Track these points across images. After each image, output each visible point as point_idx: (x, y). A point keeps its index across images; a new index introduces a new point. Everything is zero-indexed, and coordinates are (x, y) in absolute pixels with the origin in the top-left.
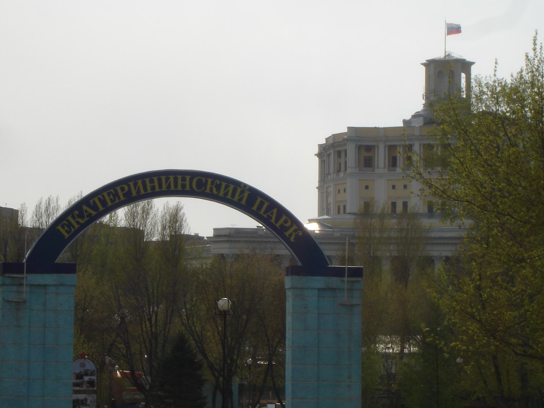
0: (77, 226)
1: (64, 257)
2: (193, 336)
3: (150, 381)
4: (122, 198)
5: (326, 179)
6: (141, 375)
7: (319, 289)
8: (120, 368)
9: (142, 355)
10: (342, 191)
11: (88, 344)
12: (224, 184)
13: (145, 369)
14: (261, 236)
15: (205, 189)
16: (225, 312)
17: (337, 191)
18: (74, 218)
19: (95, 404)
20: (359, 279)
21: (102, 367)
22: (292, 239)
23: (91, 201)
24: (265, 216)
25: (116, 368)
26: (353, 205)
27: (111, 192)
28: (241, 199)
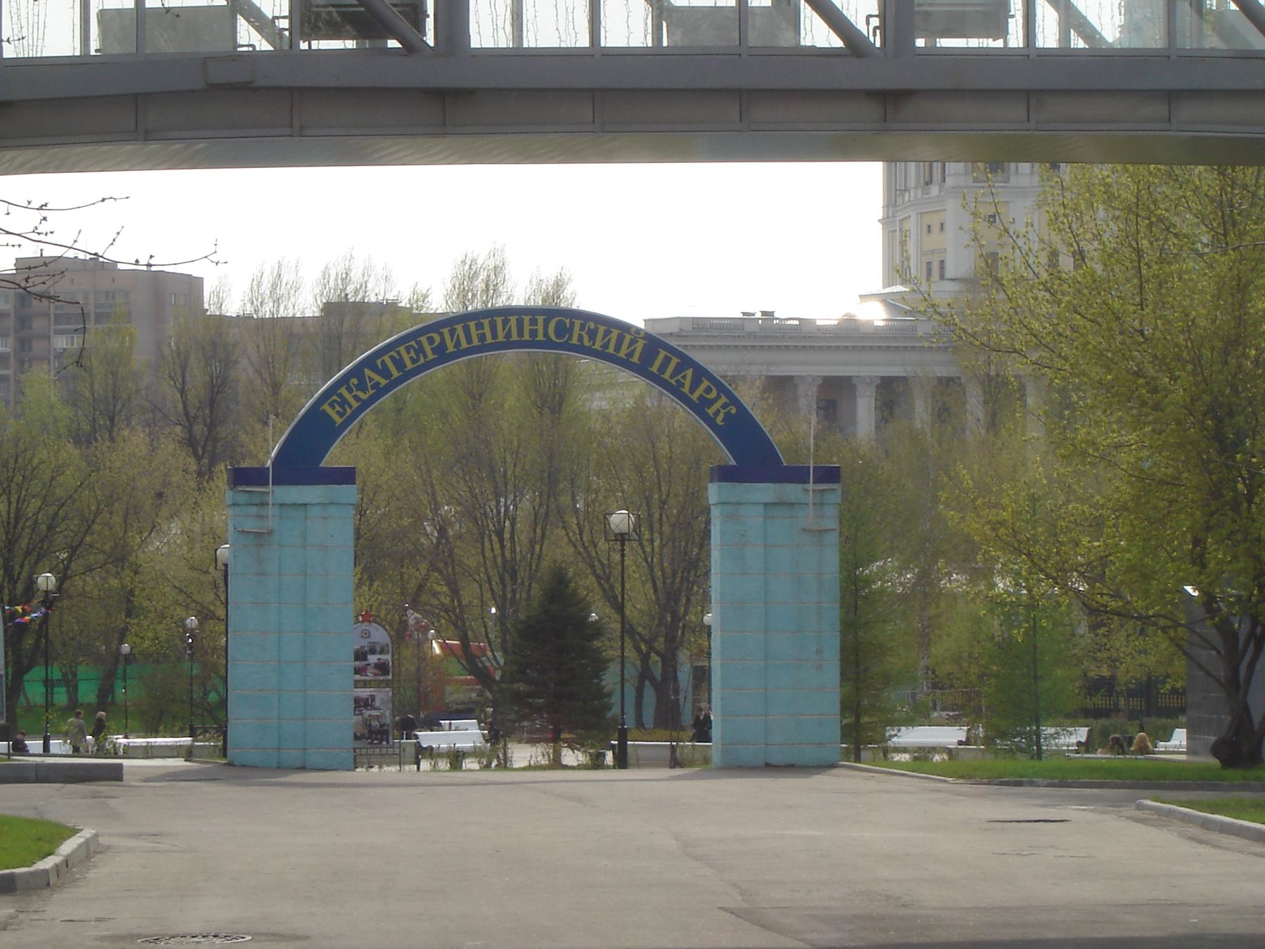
0: (355, 404)
1: (335, 457)
2: (592, 567)
3: (502, 662)
4: (431, 356)
5: (899, 200)
6: (483, 650)
7: (766, 505)
8: (439, 635)
9: (484, 606)
10: (935, 229)
11: (371, 585)
12: (602, 329)
13: (492, 636)
14: (752, 335)
15: (570, 338)
16: (622, 535)
17: (925, 230)
18: (350, 390)
19: (390, 706)
20: (835, 486)
21: (400, 633)
22: (719, 421)
23: (379, 362)
24: (673, 382)
25: (430, 636)
26: (960, 261)
27: (412, 346)
28: (631, 354)
